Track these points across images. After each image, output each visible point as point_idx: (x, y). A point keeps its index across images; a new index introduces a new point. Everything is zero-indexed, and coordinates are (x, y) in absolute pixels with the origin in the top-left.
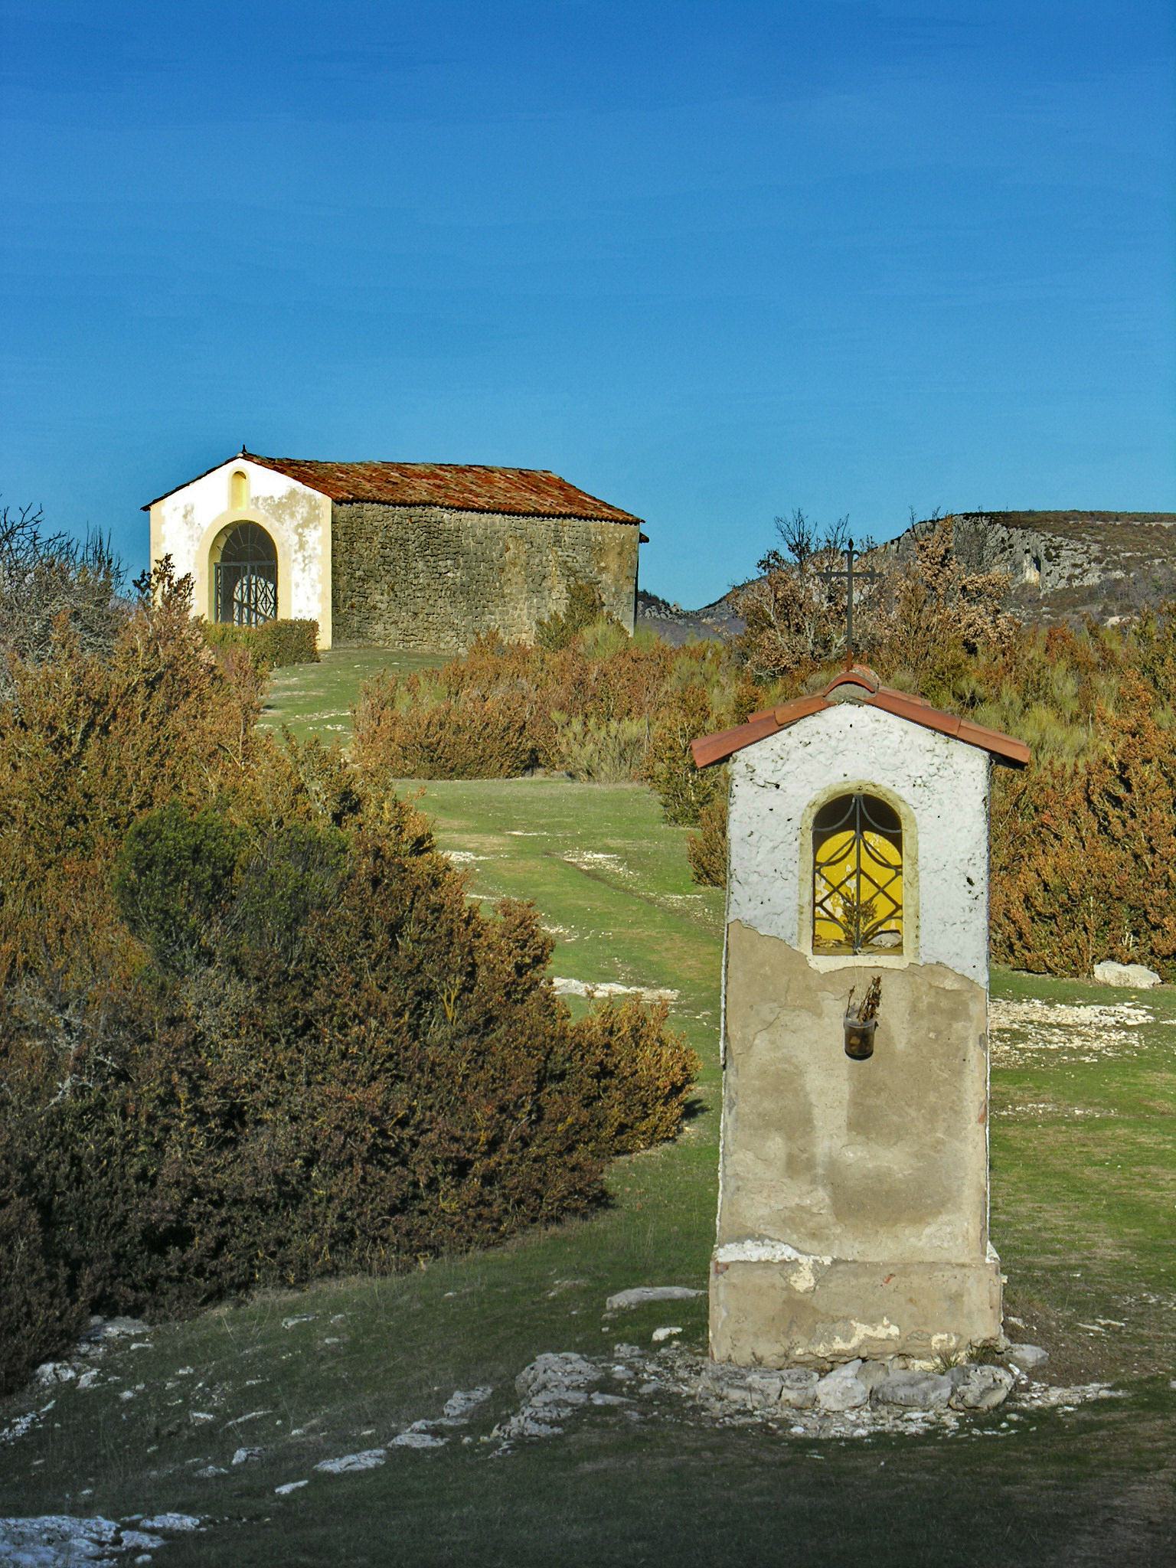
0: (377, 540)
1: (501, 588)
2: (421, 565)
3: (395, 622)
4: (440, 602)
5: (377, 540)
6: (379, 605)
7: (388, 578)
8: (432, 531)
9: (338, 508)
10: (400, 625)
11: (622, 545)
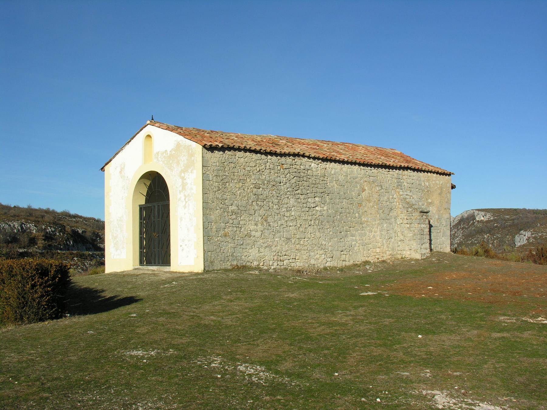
0: (250, 182)
1: (360, 217)
2: (292, 201)
3: (269, 246)
4: (310, 229)
5: (250, 182)
6: (253, 233)
7: (262, 212)
8: (301, 176)
9: (209, 154)
10: (274, 249)
11: (441, 188)
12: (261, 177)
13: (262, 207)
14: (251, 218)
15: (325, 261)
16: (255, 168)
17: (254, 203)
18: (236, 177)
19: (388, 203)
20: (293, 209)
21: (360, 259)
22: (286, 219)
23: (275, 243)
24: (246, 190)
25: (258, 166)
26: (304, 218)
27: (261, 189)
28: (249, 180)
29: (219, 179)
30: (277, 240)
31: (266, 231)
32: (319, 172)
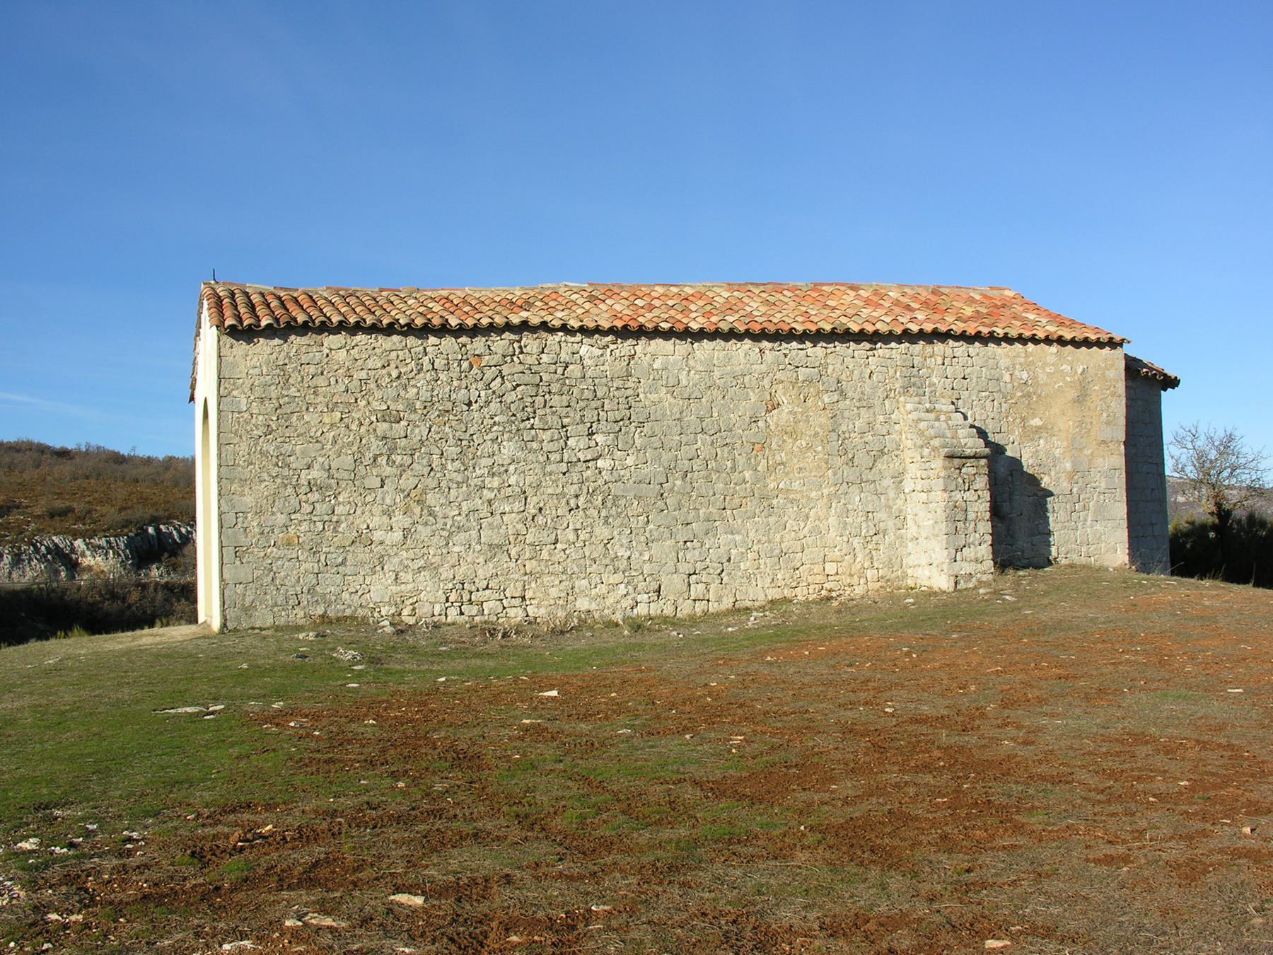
6: (378, 535)
7: (408, 481)
9: (241, 347)
10: (446, 573)
12: (402, 393)
13: (403, 469)
14: (369, 498)
15: (628, 602)
16: (384, 371)
17: (382, 460)
18: (320, 398)
19: (869, 437)
20: (512, 468)
21: (758, 592)
22: (487, 494)
23: (452, 559)
24: (354, 427)
25: (393, 365)
26: (550, 491)
27: (403, 423)
28: (364, 403)
29: (270, 406)
30: (456, 549)
31: (420, 527)
32: (606, 367)
